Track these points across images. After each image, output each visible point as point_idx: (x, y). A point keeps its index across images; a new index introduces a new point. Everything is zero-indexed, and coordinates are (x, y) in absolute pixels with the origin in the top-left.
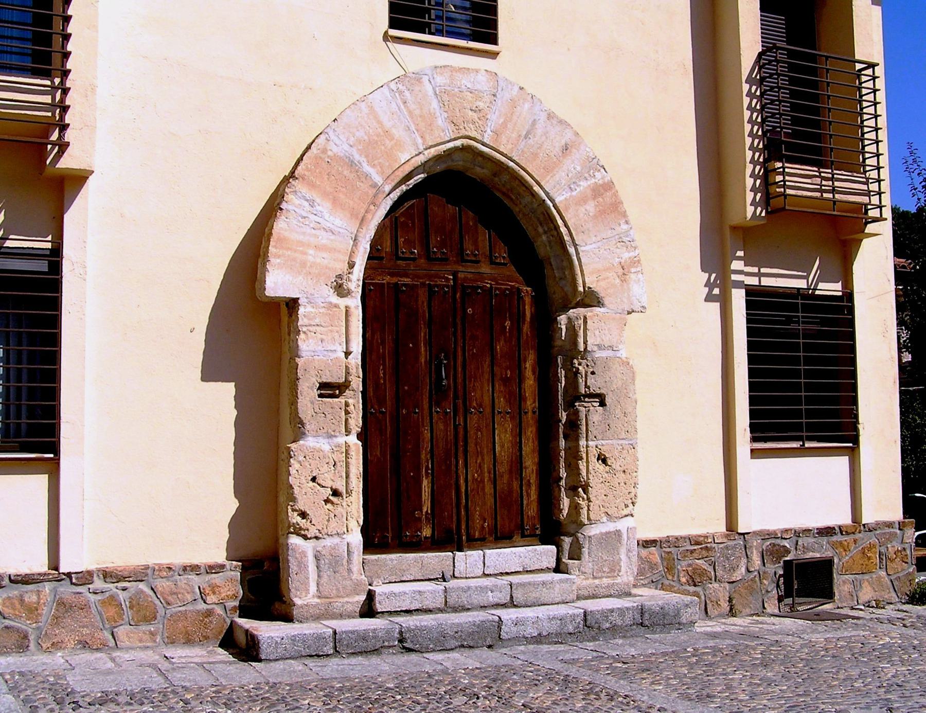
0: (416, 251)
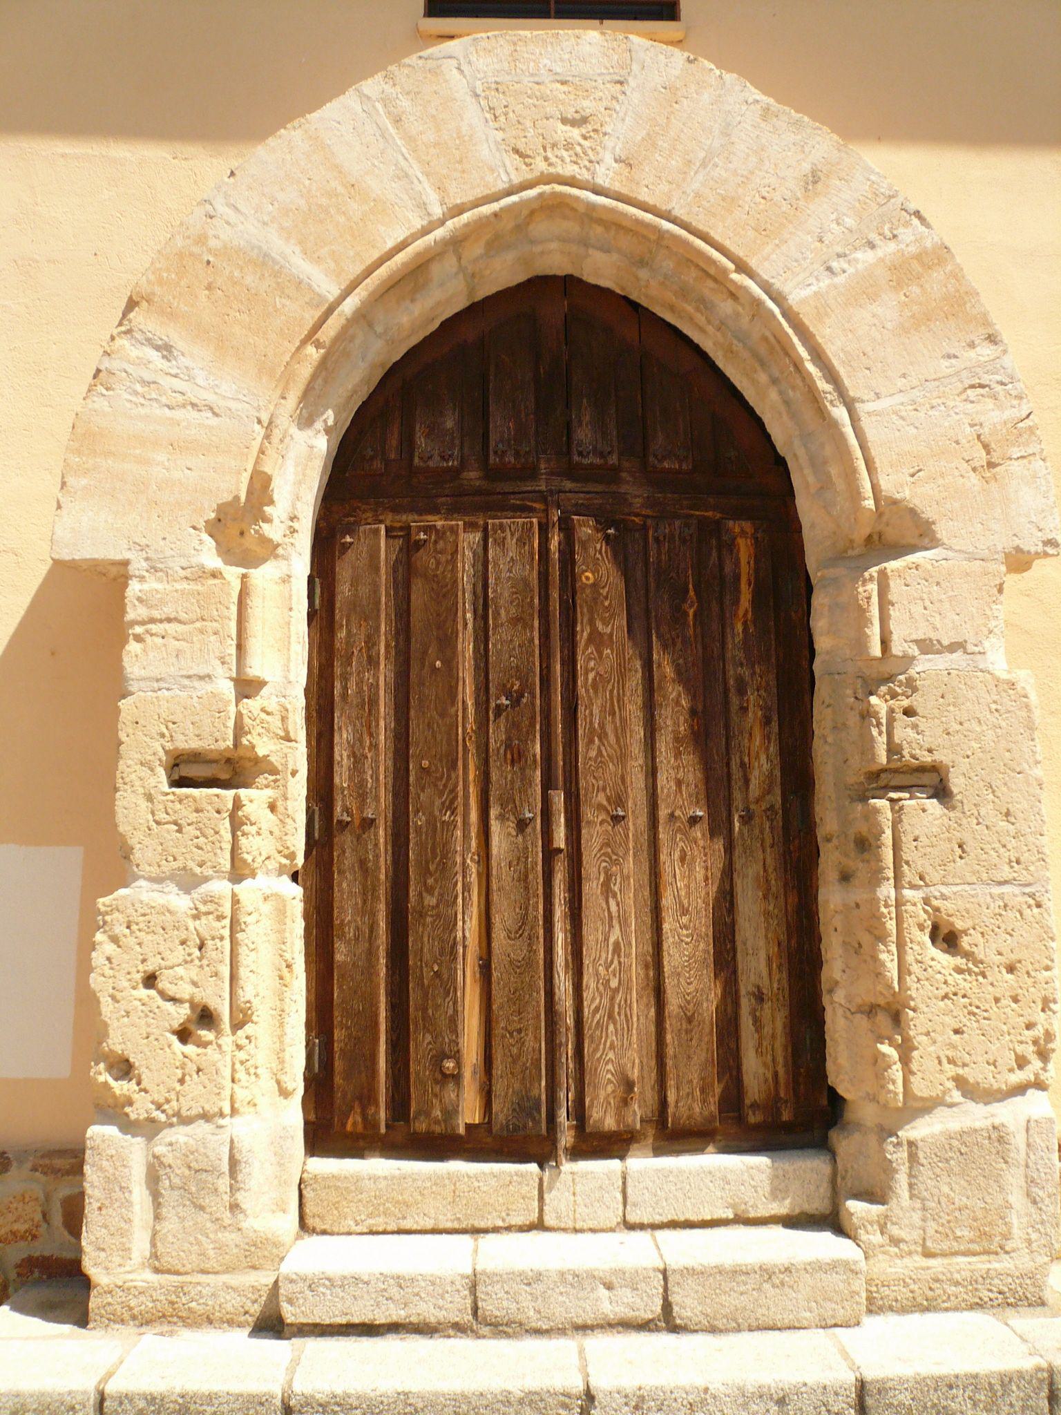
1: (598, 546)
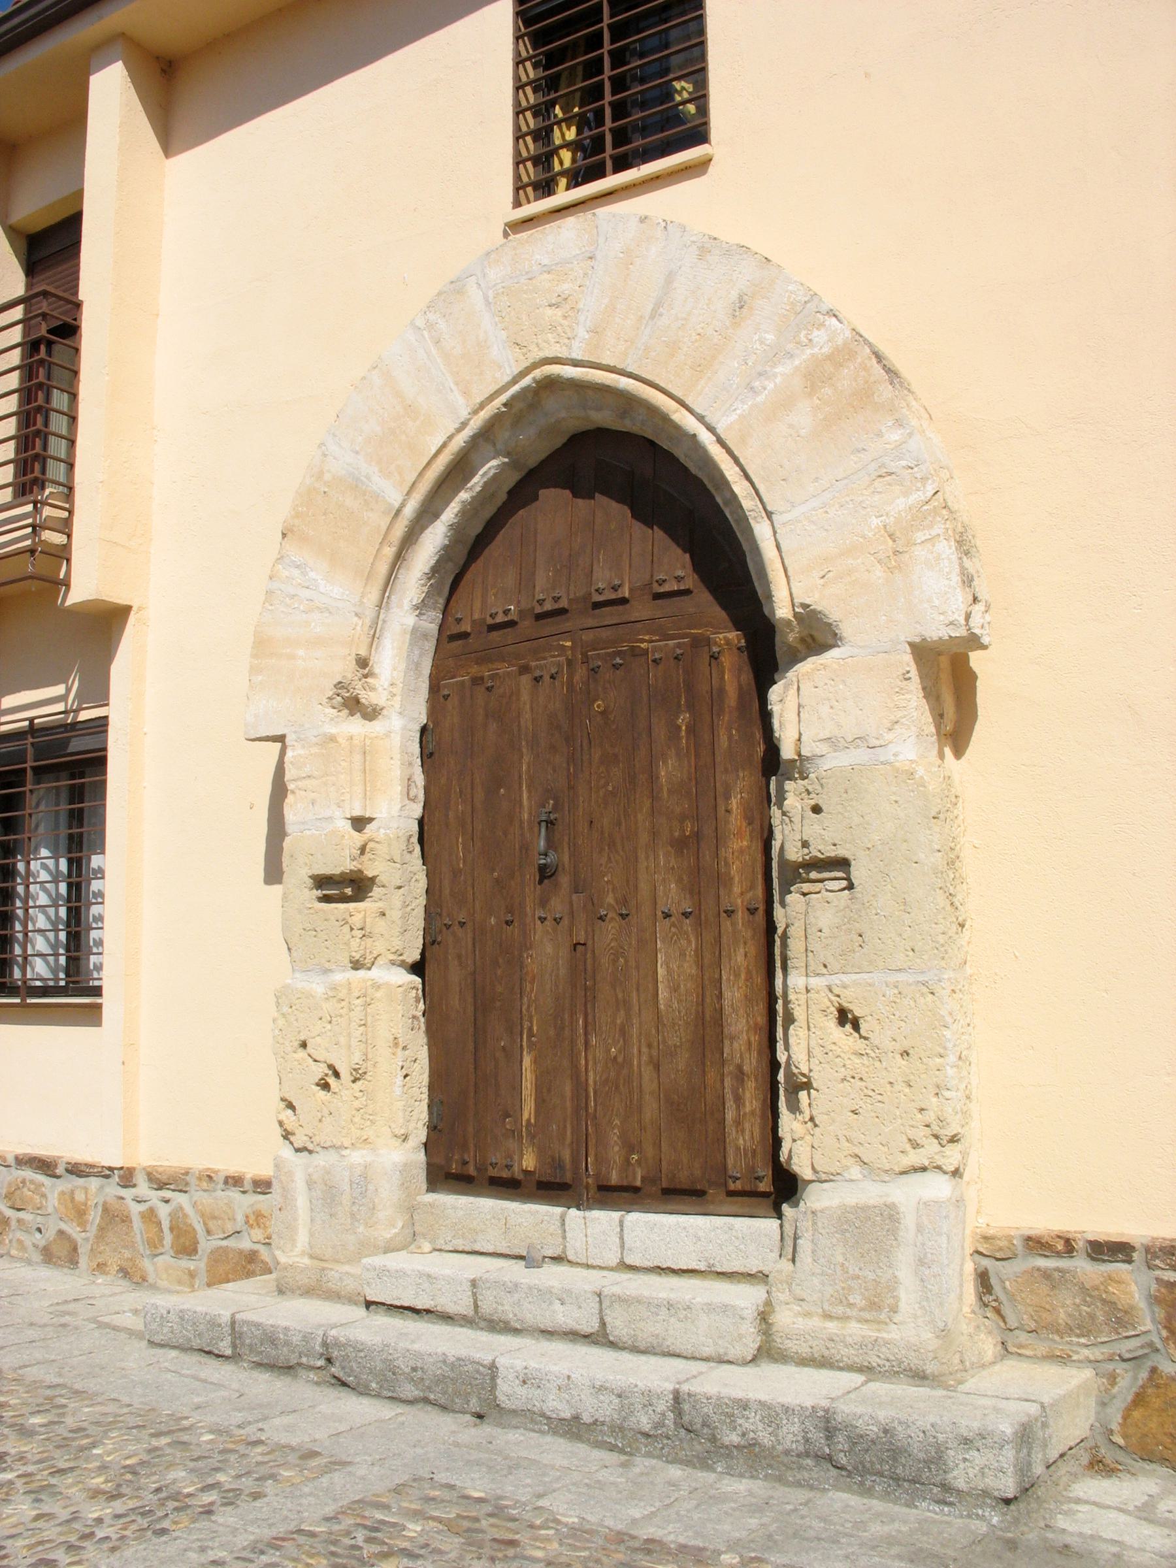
0: (512, 607)
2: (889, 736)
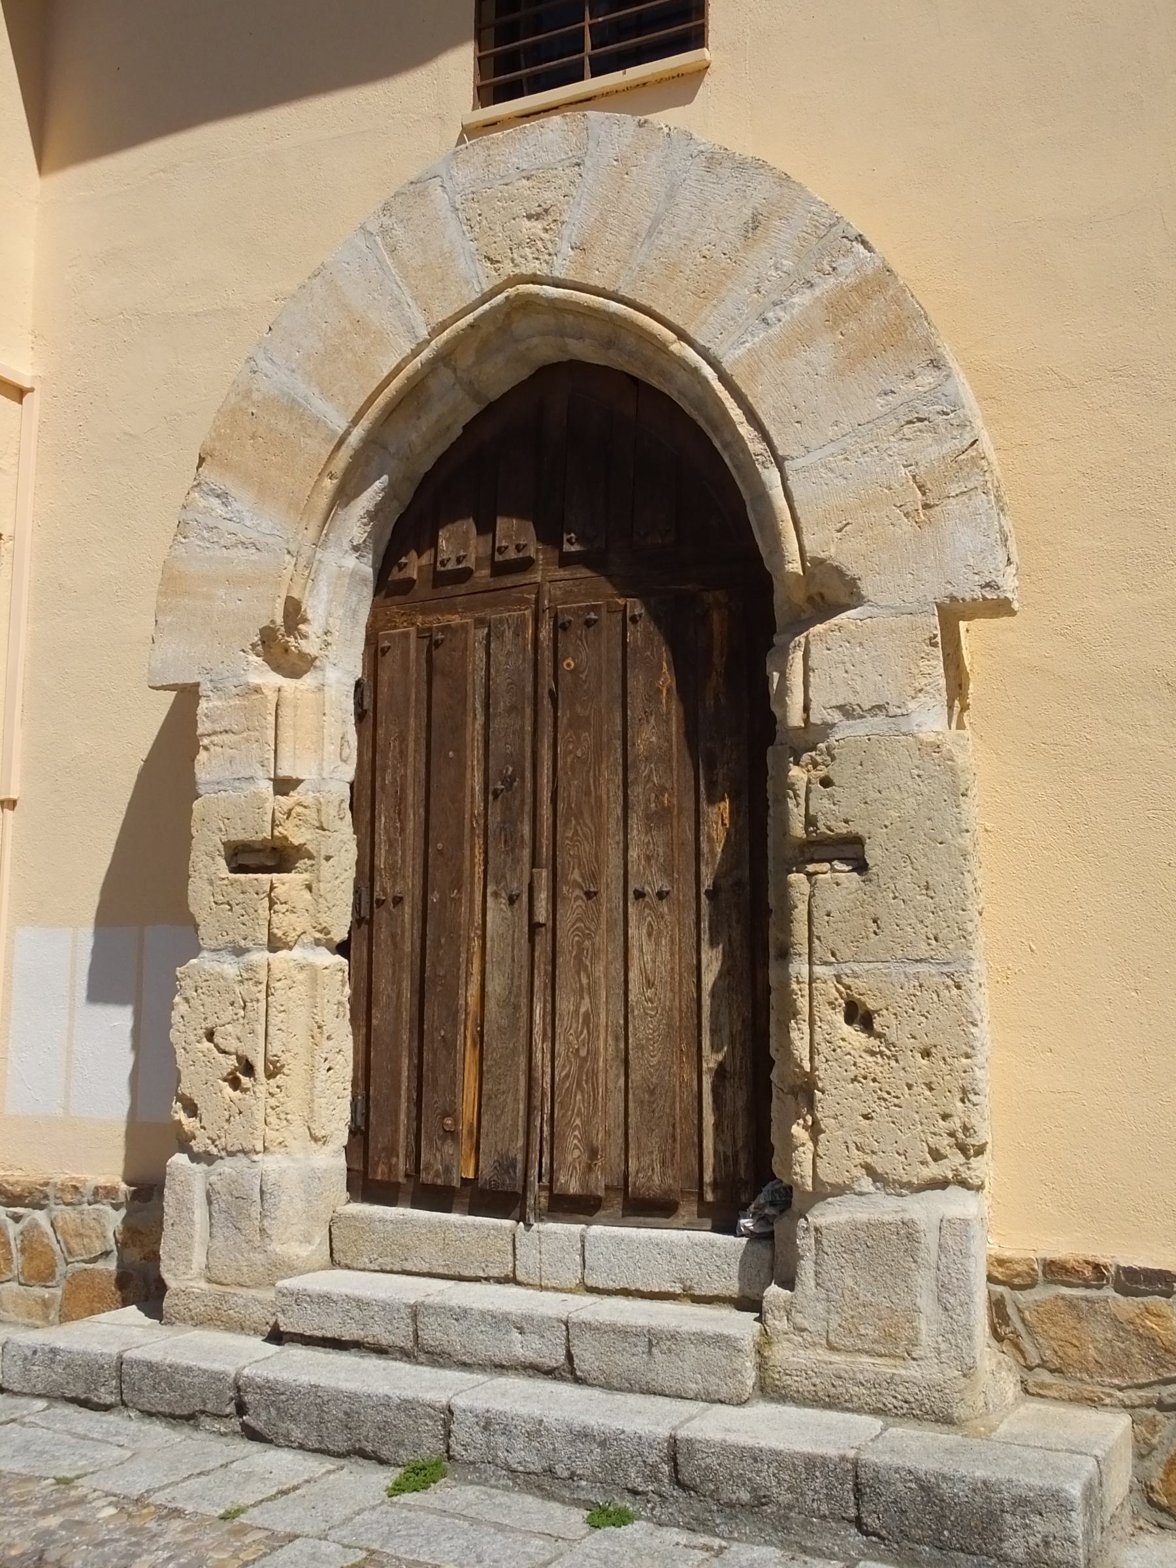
1: (579, 632)
2: (912, 705)
